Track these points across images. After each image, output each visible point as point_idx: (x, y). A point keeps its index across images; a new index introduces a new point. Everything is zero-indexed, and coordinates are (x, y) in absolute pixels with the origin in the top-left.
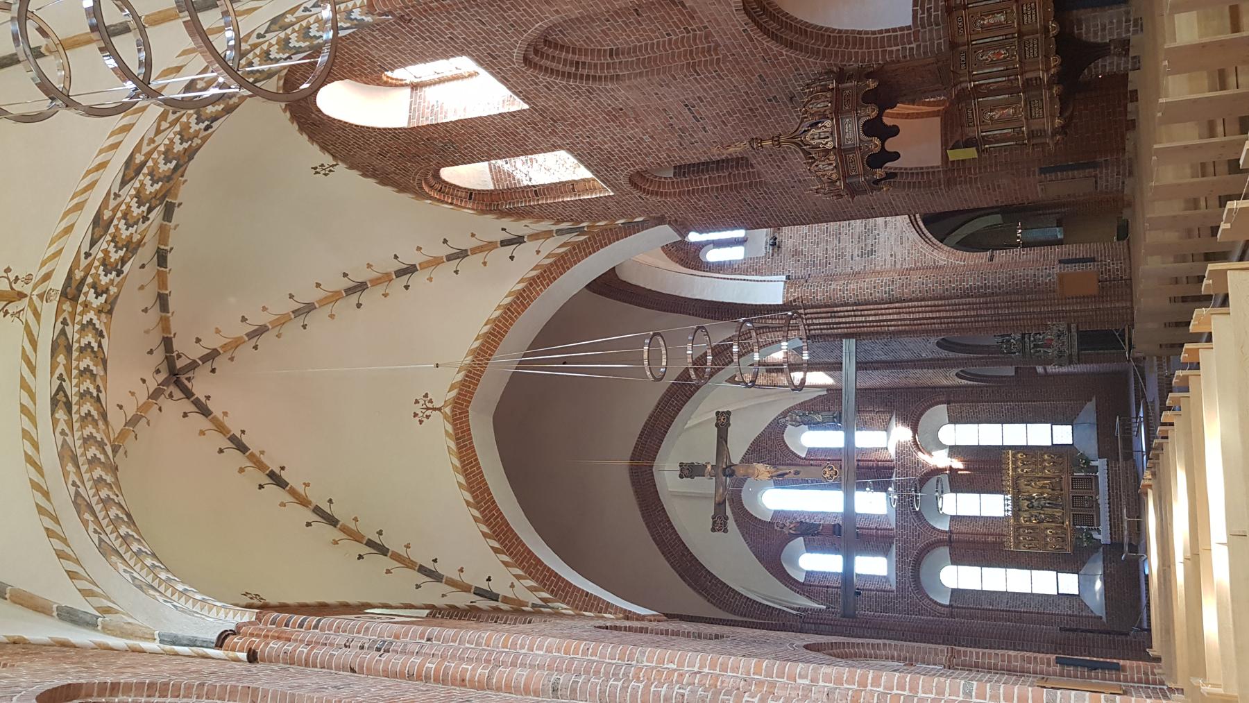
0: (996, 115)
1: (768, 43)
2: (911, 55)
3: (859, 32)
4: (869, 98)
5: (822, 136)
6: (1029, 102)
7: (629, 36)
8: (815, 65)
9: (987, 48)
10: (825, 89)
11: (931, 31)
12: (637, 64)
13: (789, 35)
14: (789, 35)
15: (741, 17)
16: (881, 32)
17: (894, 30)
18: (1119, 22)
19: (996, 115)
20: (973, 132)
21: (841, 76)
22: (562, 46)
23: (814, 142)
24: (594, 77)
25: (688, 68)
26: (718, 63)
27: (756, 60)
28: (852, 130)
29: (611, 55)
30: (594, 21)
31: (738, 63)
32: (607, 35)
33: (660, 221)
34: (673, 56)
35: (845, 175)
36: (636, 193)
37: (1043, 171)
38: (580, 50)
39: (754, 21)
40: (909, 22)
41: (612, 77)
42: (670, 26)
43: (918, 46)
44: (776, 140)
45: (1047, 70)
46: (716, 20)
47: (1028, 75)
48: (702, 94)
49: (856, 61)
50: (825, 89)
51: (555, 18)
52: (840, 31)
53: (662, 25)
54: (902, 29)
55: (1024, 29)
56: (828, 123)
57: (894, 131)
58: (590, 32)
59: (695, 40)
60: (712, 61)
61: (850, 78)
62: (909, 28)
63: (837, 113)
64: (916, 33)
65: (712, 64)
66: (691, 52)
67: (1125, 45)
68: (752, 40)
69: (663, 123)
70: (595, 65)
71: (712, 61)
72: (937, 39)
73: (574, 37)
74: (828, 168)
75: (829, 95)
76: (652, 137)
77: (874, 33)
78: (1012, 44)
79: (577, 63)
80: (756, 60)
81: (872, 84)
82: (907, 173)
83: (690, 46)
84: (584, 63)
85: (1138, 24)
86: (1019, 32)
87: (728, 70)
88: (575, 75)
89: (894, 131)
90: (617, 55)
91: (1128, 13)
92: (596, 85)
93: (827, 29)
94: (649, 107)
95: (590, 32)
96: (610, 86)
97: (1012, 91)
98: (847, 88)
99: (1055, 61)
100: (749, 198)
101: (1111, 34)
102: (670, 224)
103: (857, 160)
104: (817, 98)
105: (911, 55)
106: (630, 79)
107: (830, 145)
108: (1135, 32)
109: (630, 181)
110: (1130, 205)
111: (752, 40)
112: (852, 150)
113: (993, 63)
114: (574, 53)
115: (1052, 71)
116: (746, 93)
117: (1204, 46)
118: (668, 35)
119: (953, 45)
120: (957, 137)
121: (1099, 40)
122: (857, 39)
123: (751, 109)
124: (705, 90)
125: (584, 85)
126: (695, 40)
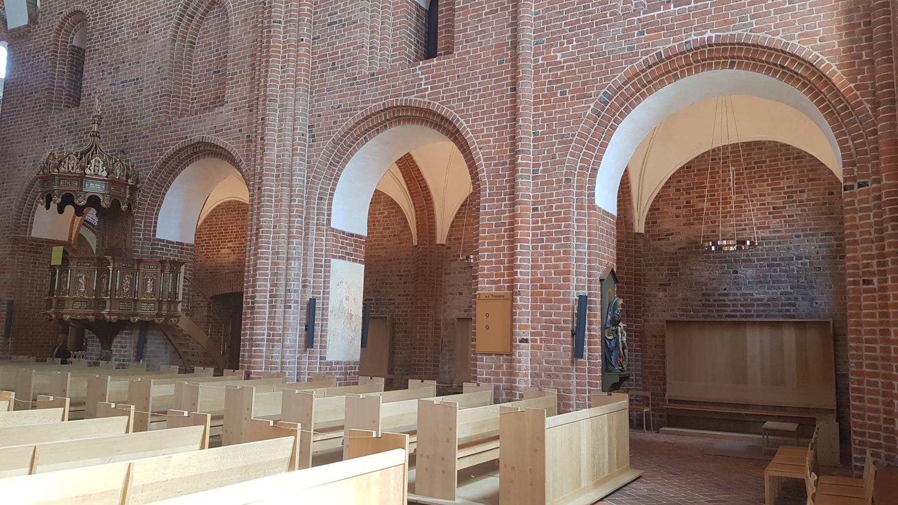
0: (82, 281)
1: (171, 149)
2: (135, 234)
3: (160, 206)
4: (116, 204)
5: (96, 167)
6: (86, 301)
7: (201, 59)
8: (146, 174)
9: (133, 281)
10: (128, 177)
11: (148, 248)
12: (179, 58)
13: (172, 163)
14: (172, 163)
15: (197, 138)
16: (156, 218)
17: (155, 227)
18: (125, 356)
19: (82, 281)
20: (73, 265)
21: (134, 189)
22: (207, 12)
23: (93, 161)
24: (179, 24)
25: (168, 91)
26: (166, 112)
27: (161, 138)
28: (95, 188)
29: (191, 42)
30: (219, 41)
31: (162, 125)
32: (206, 45)
33: (33, 19)
34: (179, 84)
35: (62, 177)
36: (66, 12)
37: (11, 304)
38: (201, 23)
39: (192, 145)
40: (157, 237)
41: (175, 36)
42: (200, 89)
43: (140, 239)
44: (96, 135)
45: (109, 314)
46: (200, 122)
47: (108, 302)
48: (144, 93)
49: (141, 199)
50: (128, 177)
51: (233, 20)
52: (164, 194)
53: (203, 84)
54: (155, 231)
55: (138, 303)
56: (105, 174)
57: (61, 210)
58: (212, 35)
59: (186, 102)
60: (168, 108)
61: (131, 194)
62: (154, 235)
63: (111, 182)
64: (149, 240)
65: (166, 108)
66: (178, 97)
67: (108, 358)
68: (178, 139)
69: (127, 57)
70: (187, 29)
71: (168, 108)
72: (141, 250)
73: (211, 22)
74: (71, 165)
75: (124, 178)
76: (117, 44)
77: (157, 214)
78: (131, 295)
79: (193, 17)
80: (161, 138)
81: (124, 207)
82: (31, 212)
83: (182, 98)
84: (191, 21)
85: (121, 366)
86: (138, 300)
87: (159, 117)
88: (185, 12)
89: (61, 210)
90: (191, 47)
91: (129, 361)
92: (173, 23)
93: (168, 187)
94: (144, 53)
95: (212, 35)
96: (169, 33)
97: (98, 291)
98: (125, 192)
99: (114, 318)
100: (37, 95)
101: (117, 351)
102: (28, 26)
103: (74, 187)
104: (124, 170)
105: (135, 234)
106: (171, 49)
107: (88, 171)
108: (89, 363)
109: (78, 12)
110: (64, 362)
111: (178, 139)
112: (81, 185)
113: (121, 283)
114: (201, 18)
115: (108, 317)
116: (136, 123)
117: (147, 399)
118: (194, 86)
119: (139, 261)
120: (71, 254)
121: (114, 344)
122: (157, 202)
123: (122, 122)
124: (147, 96)
125: (175, 15)
126: (186, 102)
